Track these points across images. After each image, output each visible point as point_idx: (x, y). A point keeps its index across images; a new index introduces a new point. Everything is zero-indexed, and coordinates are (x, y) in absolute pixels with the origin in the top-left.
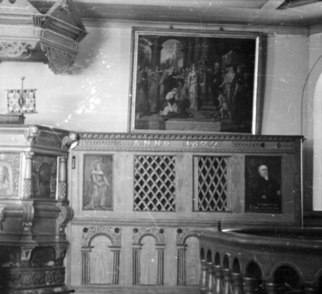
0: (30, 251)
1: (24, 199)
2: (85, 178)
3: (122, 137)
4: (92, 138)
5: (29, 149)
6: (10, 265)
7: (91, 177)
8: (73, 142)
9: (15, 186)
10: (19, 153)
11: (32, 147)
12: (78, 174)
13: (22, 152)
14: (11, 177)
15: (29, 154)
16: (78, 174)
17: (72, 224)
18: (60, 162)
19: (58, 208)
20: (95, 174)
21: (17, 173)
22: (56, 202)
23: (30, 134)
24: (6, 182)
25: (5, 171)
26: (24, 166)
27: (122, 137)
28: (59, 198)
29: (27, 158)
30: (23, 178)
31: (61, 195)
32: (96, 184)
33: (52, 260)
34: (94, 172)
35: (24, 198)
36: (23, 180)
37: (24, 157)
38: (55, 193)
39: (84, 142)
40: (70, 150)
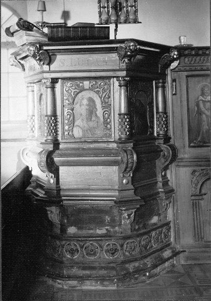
0: (134, 211)
1: (120, 142)
2: (190, 107)
3: (187, 52)
4: (197, 55)
5: (124, 73)
6: (107, 229)
7: (198, 105)
8: (174, 60)
9: (106, 123)
10: (109, 78)
11: (127, 70)
12: (181, 102)
13: (114, 77)
14: (100, 112)
15: (124, 80)
16: (181, 102)
17: (178, 166)
18: (157, 88)
19: (158, 146)
20: (203, 101)
21: (107, 106)
22: (155, 139)
23: (126, 52)
24: (93, 118)
25: (91, 104)
26: (117, 95)
27: (193, 52)
28: (158, 135)
29: (120, 86)
30: (117, 112)
31: (161, 130)
32: (205, 114)
33: (155, 215)
34: (201, 98)
35: (120, 139)
36: (117, 116)
37: (117, 84)
38: (153, 128)
39: (187, 60)
40: (169, 72)
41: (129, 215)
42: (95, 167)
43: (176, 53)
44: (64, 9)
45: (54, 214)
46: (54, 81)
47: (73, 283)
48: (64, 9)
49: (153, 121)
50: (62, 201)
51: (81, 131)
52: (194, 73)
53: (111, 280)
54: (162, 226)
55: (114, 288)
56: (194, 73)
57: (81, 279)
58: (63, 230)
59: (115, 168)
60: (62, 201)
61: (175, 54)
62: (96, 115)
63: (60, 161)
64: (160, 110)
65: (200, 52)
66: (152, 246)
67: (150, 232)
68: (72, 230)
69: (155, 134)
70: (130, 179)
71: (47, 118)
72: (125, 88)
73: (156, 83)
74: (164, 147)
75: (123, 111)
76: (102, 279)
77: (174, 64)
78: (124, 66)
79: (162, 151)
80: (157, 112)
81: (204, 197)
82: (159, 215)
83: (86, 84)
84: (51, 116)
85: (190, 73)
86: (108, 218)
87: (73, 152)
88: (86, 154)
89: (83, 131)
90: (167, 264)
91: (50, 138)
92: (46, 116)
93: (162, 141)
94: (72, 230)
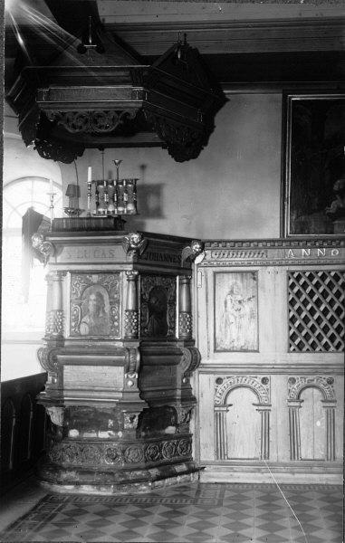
0: (137, 414)
18: (181, 284)
22: (176, 341)
24: (101, 315)
38: (174, 329)
41: (132, 419)
42: (100, 368)
43: (198, 246)
44: (19, 214)
45: (56, 416)
46: (63, 273)
47: (69, 488)
48: (19, 214)
49: (175, 322)
50: (63, 401)
51: (88, 330)
52: (225, 269)
53: (107, 485)
54: (178, 438)
55: (110, 494)
56: (225, 269)
57: (77, 484)
58: (65, 430)
59: (121, 369)
60: (63, 401)
61: (196, 247)
62: (104, 311)
63: (63, 360)
64: (184, 309)
65: (260, 245)
66: (162, 458)
67: (161, 441)
68: (73, 433)
69: (177, 336)
70: (136, 381)
71: (127, 314)
72: (133, 282)
73: (180, 279)
74: (185, 351)
75: (131, 307)
76: (97, 484)
77: (199, 259)
78: (131, 259)
79: (182, 354)
80: (180, 312)
81: (229, 408)
82: (176, 425)
83: (95, 278)
84: (133, 311)
85: (218, 269)
86: (111, 422)
87: (78, 350)
88: (93, 350)
89: (90, 328)
90: (179, 479)
91: (55, 334)
92: (126, 311)
93: (182, 344)
94: (73, 433)
